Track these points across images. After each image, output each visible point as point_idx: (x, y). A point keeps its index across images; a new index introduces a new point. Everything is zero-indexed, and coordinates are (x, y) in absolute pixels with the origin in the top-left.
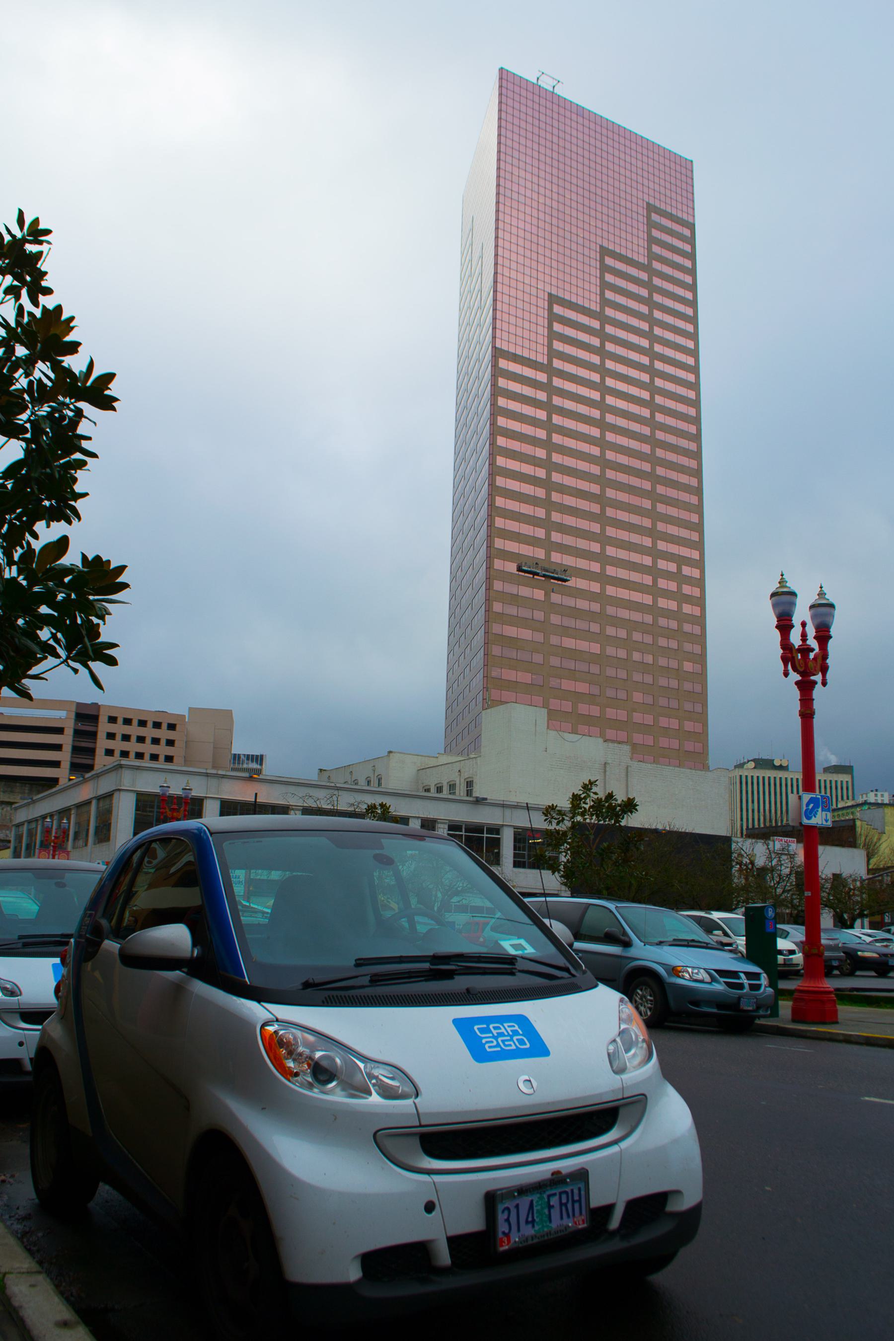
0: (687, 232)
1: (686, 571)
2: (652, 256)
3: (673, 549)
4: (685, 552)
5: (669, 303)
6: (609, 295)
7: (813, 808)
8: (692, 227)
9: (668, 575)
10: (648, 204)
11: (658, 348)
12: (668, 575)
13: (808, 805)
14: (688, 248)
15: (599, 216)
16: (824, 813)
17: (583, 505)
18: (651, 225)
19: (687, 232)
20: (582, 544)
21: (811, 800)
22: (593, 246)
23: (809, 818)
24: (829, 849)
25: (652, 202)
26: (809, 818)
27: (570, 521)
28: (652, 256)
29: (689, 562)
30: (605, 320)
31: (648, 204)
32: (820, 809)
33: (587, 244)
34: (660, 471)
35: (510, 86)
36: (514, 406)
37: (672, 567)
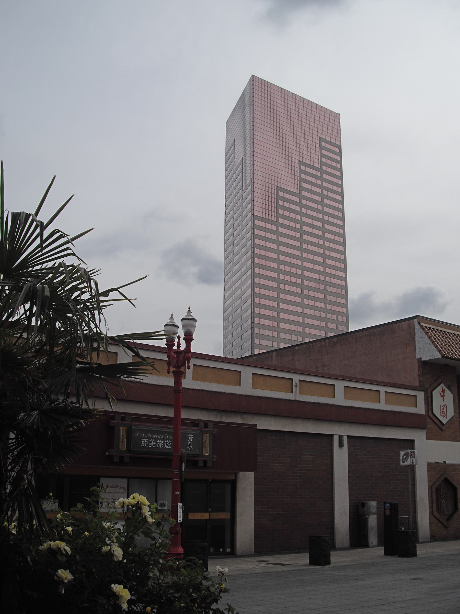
0: (338, 150)
1: (340, 318)
2: (322, 164)
3: (334, 308)
4: (339, 309)
5: (330, 186)
6: (324, 152)
7: (406, 458)
8: (340, 147)
9: (332, 321)
10: (320, 137)
11: (326, 209)
12: (332, 321)
13: (403, 456)
14: (338, 158)
15: (266, 108)
16: (411, 459)
17: (294, 289)
18: (321, 148)
19: (338, 150)
20: (294, 308)
21: (405, 454)
22: (296, 161)
23: (404, 462)
24: (355, 290)
25: (321, 136)
26: (404, 462)
27: (288, 297)
28: (322, 164)
29: (340, 313)
30: (302, 197)
31: (320, 137)
32: (409, 458)
33: (293, 160)
34: (328, 270)
35: (257, 84)
36: (262, 243)
37: (334, 317)
